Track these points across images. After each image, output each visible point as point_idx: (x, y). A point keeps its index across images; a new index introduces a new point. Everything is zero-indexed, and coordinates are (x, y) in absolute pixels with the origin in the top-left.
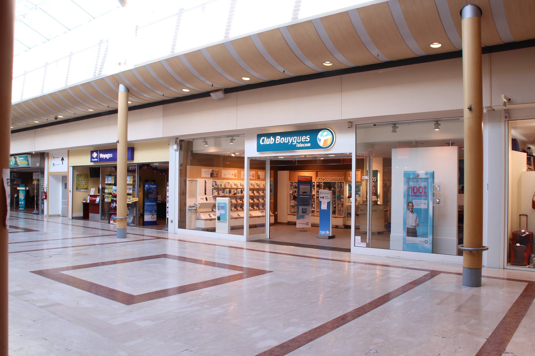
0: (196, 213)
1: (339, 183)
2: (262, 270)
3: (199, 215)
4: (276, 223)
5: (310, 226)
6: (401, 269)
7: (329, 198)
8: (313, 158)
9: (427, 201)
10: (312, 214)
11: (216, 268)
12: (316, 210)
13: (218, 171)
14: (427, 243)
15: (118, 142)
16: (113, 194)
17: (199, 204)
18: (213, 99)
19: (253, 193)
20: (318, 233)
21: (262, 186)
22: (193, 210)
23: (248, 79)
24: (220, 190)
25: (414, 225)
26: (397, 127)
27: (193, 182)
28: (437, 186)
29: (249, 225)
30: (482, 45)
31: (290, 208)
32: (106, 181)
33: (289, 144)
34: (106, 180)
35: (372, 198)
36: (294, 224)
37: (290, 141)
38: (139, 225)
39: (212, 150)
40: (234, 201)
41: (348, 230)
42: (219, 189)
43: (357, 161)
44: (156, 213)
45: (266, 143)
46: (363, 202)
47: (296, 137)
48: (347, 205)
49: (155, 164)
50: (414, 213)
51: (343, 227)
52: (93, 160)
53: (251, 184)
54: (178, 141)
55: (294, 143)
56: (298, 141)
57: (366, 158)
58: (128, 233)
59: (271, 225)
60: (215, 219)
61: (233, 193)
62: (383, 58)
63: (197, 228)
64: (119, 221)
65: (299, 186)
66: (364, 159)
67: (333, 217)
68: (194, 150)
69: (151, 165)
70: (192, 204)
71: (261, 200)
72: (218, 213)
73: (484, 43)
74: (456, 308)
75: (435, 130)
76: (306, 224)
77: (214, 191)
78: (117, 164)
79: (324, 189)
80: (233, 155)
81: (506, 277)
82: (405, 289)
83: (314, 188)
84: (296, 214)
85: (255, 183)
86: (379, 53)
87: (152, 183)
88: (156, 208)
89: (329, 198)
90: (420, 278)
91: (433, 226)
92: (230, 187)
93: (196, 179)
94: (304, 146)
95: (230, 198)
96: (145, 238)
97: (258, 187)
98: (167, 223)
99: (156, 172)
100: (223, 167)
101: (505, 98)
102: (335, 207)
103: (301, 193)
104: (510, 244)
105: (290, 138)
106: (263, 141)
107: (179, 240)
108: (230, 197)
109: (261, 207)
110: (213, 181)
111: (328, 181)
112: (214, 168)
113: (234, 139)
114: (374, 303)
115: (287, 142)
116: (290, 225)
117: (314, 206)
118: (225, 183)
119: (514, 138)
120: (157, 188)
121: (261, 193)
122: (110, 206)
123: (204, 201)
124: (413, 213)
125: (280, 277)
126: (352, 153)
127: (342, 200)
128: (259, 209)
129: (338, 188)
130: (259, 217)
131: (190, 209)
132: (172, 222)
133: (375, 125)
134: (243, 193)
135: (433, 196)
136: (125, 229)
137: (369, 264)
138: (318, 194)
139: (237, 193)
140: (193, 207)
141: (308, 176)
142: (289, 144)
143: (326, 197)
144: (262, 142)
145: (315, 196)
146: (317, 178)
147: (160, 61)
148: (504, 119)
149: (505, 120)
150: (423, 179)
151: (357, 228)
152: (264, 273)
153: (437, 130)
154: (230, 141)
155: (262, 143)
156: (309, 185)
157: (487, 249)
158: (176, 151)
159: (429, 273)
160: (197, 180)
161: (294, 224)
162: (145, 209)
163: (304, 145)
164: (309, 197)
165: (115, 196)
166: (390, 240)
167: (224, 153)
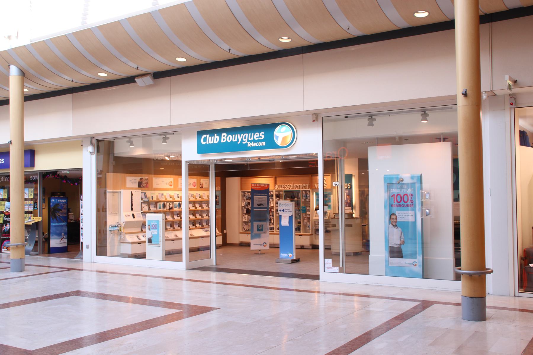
0: (120, 234)
1: (304, 192)
2: (205, 307)
3: (124, 237)
4: (225, 244)
5: (268, 247)
6: (384, 300)
7: (290, 211)
8: (269, 160)
9: (413, 212)
10: (270, 232)
11: (147, 306)
12: (276, 227)
13: (147, 179)
14: (415, 265)
15: (11, 143)
16: (5, 213)
17: (124, 222)
18: (138, 86)
19: (194, 206)
20: (278, 255)
21: (206, 197)
22: (116, 231)
23: (183, 60)
24: (151, 204)
25: (399, 242)
26: (375, 120)
27: (115, 194)
28: (426, 193)
29: (189, 248)
30: (480, 12)
31: (242, 225)
33: (238, 143)
35: (345, 210)
36: (248, 245)
37: (240, 140)
38: (43, 253)
39: (139, 152)
40: (169, 218)
41: (316, 250)
42: (150, 203)
43: (325, 163)
44: (67, 237)
45: (209, 142)
46: (335, 214)
47: (247, 135)
48: (314, 219)
49: (63, 172)
50: (397, 228)
51: (311, 247)
53: (192, 195)
54: (94, 142)
55: (245, 141)
56: (250, 139)
57: (337, 159)
58: (26, 265)
59: (217, 247)
60: (145, 242)
61: (168, 207)
62: (355, 32)
63: (121, 254)
64: (13, 248)
65: (253, 197)
66: (334, 160)
67: (296, 235)
68: (115, 152)
69: (58, 173)
70: (114, 223)
71: (204, 215)
72: (149, 234)
73: (482, 10)
74: (454, 350)
75: (422, 122)
76: (263, 245)
77: (143, 205)
78: (9, 173)
79: (285, 199)
80: (167, 158)
81: (518, 307)
82: (389, 326)
83: (272, 199)
84: (250, 232)
85: (197, 194)
86: (351, 25)
87: (61, 197)
88: (67, 229)
89: (291, 212)
90: (407, 311)
91: (423, 243)
92: (163, 199)
93: (120, 191)
94: (257, 145)
95: (164, 214)
96: (51, 270)
97: (200, 199)
98: (81, 249)
99: (65, 182)
100: (154, 174)
101: (510, 80)
102: (299, 223)
103: (255, 205)
104: (521, 265)
105: (239, 135)
106: (205, 139)
107: (98, 271)
108: (165, 213)
109: (205, 224)
110: (141, 193)
111: (289, 189)
112: (143, 175)
113: (168, 138)
114: (349, 345)
115: (236, 140)
116: (243, 246)
117: (272, 222)
118: (158, 194)
119: (522, 130)
120: (67, 203)
121: (205, 207)
122: (2, 229)
123: (131, 219)
124: (396, 227)
125: (228, 316)
126: (318, 153)
127: (308, 213)
128: (202, 227)
129: (303, 198)
130: (202, 237)
131: (112, 229)
132: (87, 247)
133: (346, 117)
134: (181, 207)
135: (422, 205)
136: (21, 259)
137: (344, 294)
138: (278, 206)
139: (173, 207)
140: (116, 226)
141: (264, 184)
142: (238, 143)
143: (287, 209)
144: (204, 141)
145: (273, 208)
146: (276, 186)
147: (65, 35)
148: (508, 106)
149: (510, 108)
150: (410, 184)
151: (327, 249)
152: (208, 311)
153: (425, 122)
154: (162, 140)
155: (203, 143)
156: (266, 194)
157: (492, 271)
158: (91, 155)
159: (419, 304)
160: (120, 192)
161: (248, 245)
162: (51, 231)
163: (258, 144)
164: (266, 210)
165: (8, 216)
166: (369, 262)
167: (156, 156)
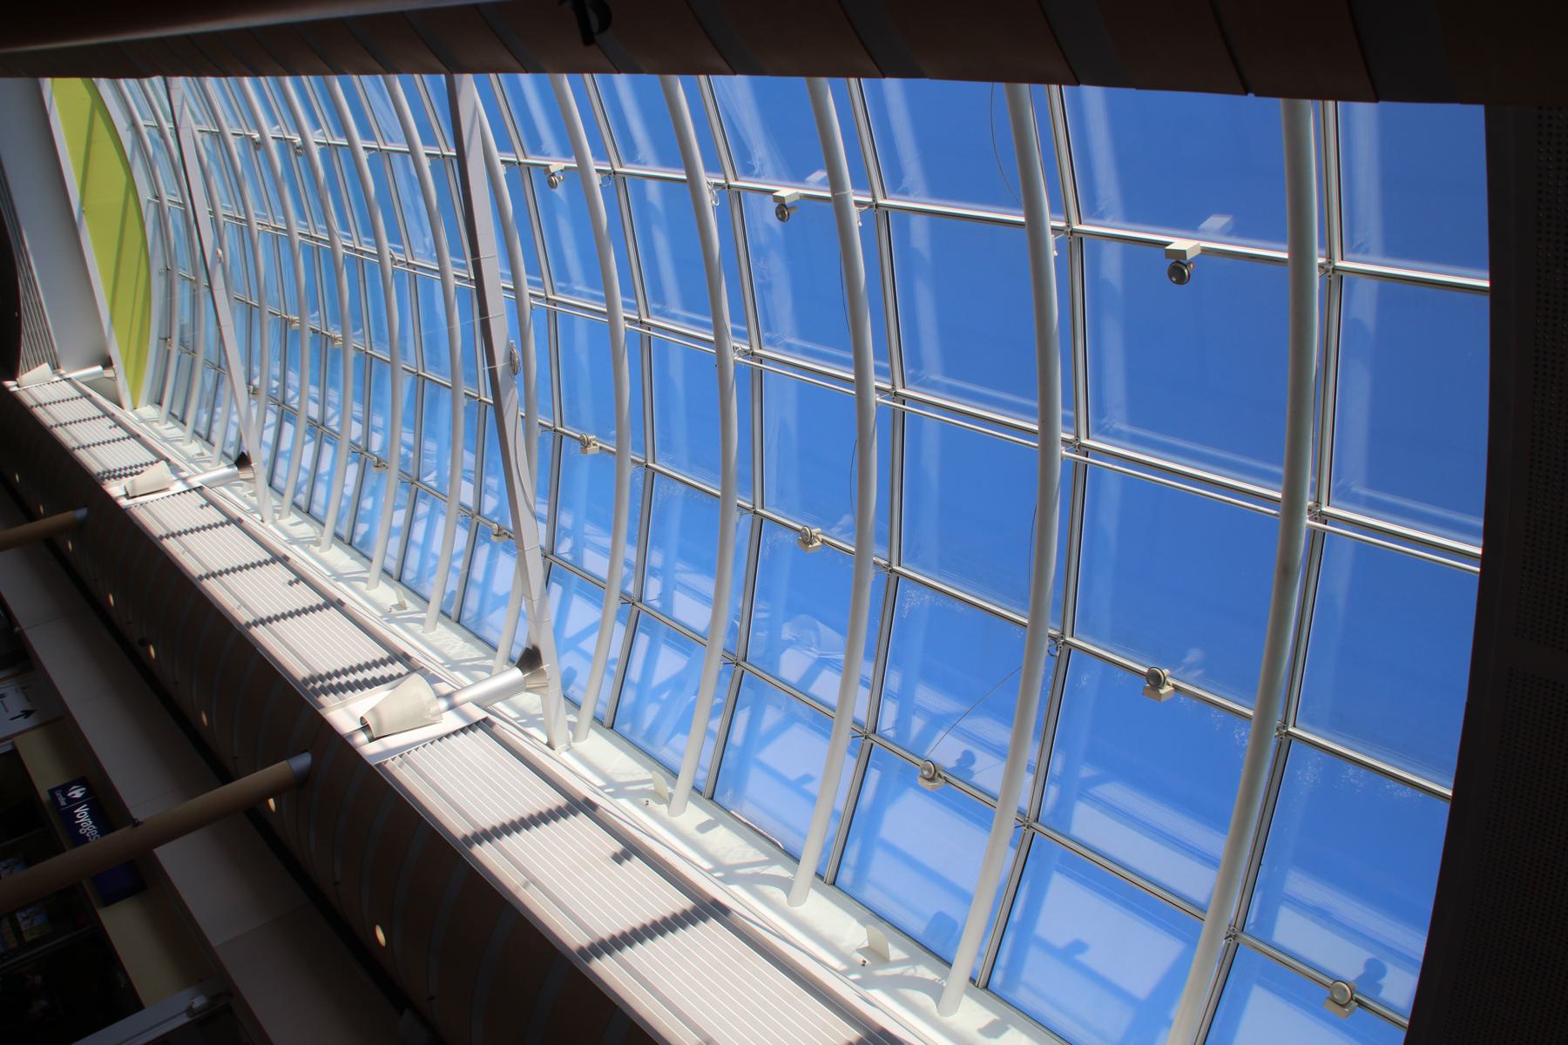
32: (24, 915)
34: (9, 861)
52: (58, 794)
